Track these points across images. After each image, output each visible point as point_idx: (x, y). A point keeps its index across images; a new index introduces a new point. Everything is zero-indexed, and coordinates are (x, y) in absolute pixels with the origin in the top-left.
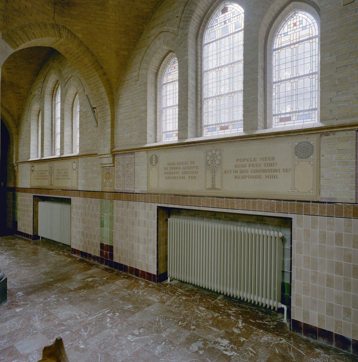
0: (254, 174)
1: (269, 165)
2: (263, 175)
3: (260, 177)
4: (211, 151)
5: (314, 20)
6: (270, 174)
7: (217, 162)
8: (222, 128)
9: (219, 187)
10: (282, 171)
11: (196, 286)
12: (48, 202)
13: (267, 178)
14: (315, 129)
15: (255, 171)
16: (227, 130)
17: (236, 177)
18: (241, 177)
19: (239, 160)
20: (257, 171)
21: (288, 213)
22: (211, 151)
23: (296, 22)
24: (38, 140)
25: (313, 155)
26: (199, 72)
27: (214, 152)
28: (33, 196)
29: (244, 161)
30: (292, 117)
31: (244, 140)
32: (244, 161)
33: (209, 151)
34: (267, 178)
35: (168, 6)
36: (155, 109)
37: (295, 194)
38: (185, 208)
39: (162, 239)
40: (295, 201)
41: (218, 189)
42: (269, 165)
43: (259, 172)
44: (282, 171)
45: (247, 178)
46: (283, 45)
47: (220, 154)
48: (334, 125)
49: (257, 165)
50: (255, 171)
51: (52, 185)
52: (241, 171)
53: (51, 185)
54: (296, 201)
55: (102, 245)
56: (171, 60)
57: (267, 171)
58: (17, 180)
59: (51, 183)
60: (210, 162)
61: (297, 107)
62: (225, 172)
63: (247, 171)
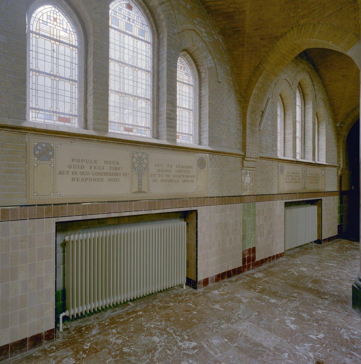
0: (95, 177)
1: (114, 169)
2: (106, 178)
3: (102, 180)
4: (137, 153)
5: (33, 16)
6: (112, 177)
7: (144, 166)
8: (60, 119)
9: (146, 190)
10: (122, 175)
11: (139, 298)
12: (170, 221)
13: (110, 181)
14: (33, 129)
15: (96, 174)
16: (69, 124)
17: (73, 179)
18: (80, 179)
19: (75, 160)
20: (99, 174)
21: (27, 219)
22: (137, 153)
23: (53, 18)
24: (318, 148)
25: (54, 158)
26: (156, 76)
27: (140, 154)
28: (285, 203)
29: (82, 162)
30: (71, 119)
31: (160, 148)
32: (82, 162)
33: (135, 152)
34: (110, 181)
35: (308, 84)
36: (200, 112)
37: (58, 197)
38: (134, 214)
39: (113, 258)
40: (35, 205)
41: (145, 192)
42: (114, 169)
43: (100, 175)
44: (122, 175)
45: (88, 181)
46: (41, 33)
47: (146, 158)
48: (8, 125)
49: (100, 168)
50: (96, 174)
51: (305, 188)
52: (81, 173)
53: (305, 188)
54: (67, 204)
55: (254, 250)
56: (190, 66)
57: (109, 174)
58: (338, 184)
59: (305, 186)
60: (136, 165)
61: (37, 104)
62: (60, 173)
63: (88, 174)
